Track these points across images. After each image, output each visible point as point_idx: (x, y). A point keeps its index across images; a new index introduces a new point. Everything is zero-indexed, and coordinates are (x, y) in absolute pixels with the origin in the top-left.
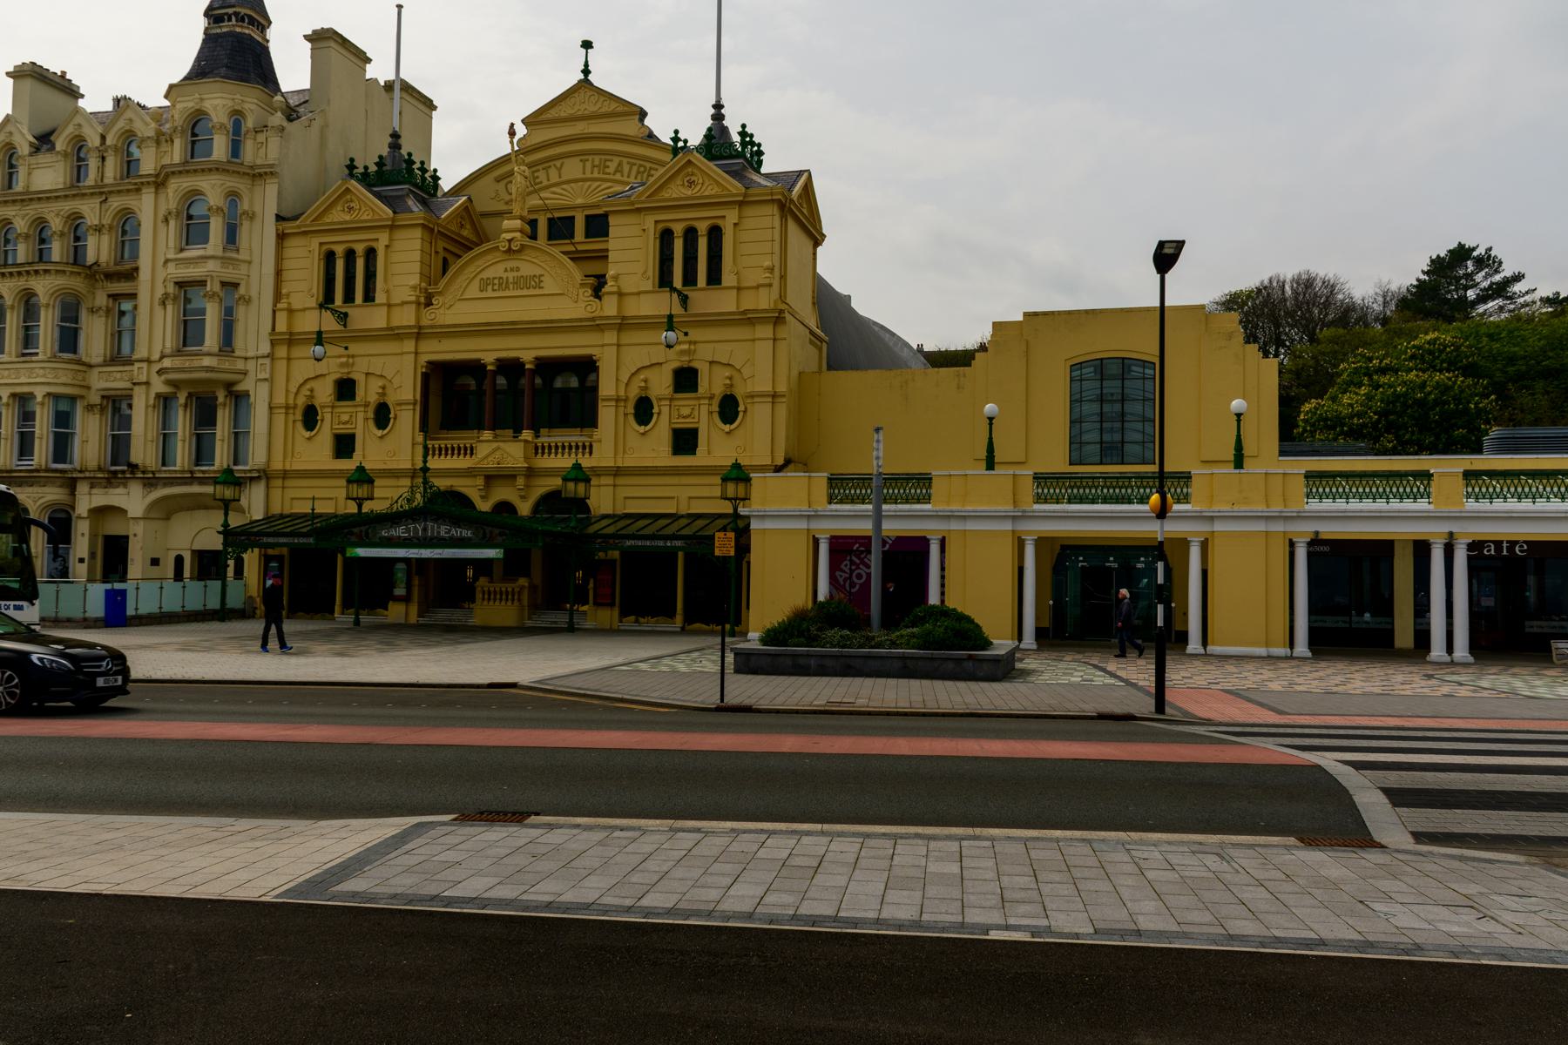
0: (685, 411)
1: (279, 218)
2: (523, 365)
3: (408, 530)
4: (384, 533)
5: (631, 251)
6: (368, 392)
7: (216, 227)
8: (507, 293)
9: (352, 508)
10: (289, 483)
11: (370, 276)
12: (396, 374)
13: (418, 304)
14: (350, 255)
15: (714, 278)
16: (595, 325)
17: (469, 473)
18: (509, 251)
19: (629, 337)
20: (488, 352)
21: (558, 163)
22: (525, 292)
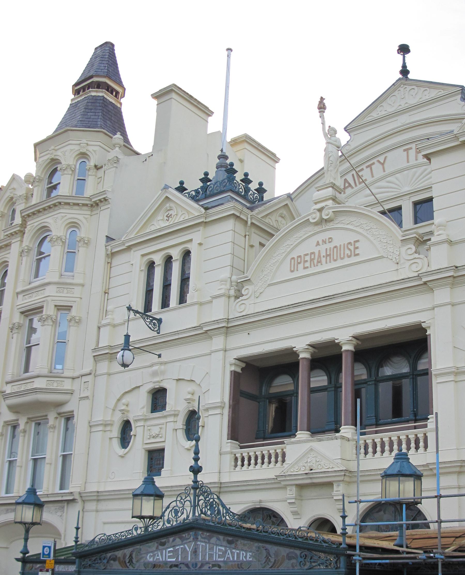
0: (155, 431)
1: (109, 239)
2: (338, 346)
4: (149, 559)
6: (177, 403)
8: (320, 268)
10: (103, 506)
12: (207, 380)
17: (277, 484)
20: (300, 338)
21: (381, 159)
22: (339, 263)
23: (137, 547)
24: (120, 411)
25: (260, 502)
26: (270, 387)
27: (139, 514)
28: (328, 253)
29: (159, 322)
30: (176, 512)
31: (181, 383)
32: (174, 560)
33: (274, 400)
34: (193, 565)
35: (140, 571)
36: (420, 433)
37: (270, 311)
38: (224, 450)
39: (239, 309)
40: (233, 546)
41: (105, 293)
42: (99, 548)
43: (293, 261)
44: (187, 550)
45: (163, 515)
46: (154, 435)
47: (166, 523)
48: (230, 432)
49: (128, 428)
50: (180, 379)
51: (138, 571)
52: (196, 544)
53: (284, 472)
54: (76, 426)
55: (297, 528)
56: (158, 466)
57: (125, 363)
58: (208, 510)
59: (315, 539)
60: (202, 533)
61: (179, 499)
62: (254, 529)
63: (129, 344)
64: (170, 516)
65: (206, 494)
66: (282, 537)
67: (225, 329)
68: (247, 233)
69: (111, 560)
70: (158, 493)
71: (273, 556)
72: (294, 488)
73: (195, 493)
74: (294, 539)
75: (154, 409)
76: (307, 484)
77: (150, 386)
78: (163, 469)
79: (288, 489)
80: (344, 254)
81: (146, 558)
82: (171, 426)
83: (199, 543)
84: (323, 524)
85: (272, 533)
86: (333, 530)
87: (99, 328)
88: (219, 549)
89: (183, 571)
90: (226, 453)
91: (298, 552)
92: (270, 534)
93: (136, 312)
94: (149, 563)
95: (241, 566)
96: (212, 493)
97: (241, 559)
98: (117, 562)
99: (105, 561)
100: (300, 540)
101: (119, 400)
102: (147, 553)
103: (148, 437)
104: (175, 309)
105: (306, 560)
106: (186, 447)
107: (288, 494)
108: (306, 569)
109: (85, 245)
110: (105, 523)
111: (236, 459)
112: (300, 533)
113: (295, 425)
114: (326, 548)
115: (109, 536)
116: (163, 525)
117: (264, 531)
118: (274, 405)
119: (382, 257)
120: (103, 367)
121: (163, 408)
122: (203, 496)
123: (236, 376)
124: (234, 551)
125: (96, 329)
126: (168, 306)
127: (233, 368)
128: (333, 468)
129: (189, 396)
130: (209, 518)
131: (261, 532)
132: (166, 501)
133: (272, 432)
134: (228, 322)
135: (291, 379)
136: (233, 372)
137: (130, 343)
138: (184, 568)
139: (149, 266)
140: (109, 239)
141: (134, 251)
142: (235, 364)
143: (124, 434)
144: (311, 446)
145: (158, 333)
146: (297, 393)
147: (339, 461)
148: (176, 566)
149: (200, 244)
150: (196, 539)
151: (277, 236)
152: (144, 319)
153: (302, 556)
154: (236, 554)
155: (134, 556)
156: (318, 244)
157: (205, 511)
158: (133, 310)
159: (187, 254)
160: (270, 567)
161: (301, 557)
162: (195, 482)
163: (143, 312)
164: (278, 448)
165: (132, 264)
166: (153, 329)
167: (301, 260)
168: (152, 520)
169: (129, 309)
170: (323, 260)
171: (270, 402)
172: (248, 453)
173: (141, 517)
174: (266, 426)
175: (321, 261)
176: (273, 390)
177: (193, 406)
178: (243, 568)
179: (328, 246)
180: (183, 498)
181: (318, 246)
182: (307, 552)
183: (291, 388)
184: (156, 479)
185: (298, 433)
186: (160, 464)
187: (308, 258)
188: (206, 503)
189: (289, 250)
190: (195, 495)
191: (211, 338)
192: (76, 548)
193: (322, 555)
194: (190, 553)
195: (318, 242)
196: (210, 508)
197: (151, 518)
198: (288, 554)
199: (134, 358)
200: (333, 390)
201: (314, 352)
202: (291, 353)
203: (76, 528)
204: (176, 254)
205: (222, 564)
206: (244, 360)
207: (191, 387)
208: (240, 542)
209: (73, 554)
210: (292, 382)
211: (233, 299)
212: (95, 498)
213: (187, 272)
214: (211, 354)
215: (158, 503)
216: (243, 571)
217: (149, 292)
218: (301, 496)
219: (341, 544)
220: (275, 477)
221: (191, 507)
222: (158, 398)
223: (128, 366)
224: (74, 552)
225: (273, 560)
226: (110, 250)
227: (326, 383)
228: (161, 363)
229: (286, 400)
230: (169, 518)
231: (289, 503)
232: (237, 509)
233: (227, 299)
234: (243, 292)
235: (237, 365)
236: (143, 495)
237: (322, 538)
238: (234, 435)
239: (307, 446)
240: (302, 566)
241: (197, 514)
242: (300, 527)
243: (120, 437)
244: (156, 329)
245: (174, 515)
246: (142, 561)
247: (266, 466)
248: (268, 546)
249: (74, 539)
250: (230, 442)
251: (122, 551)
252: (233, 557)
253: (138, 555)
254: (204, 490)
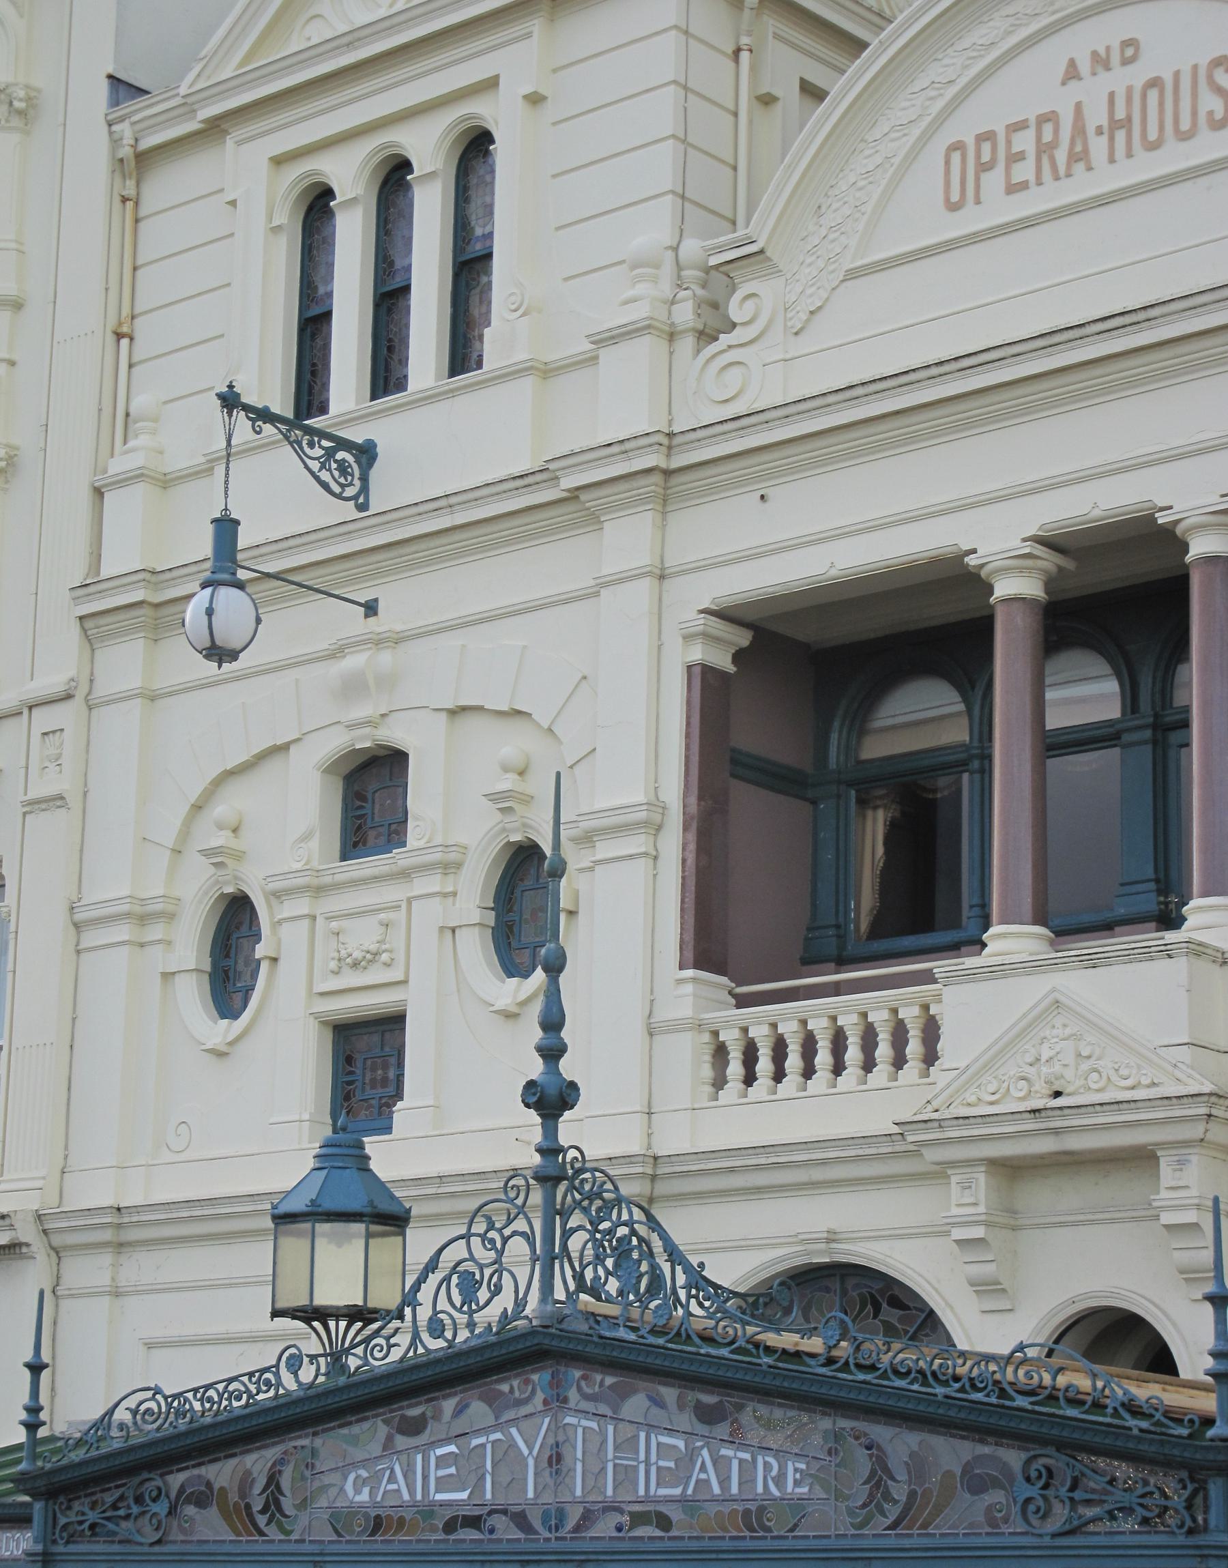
1: (122, 89)
3: (468, 1463)
6: (458, 816)
10: (141, 1268)
11: (470, 267)
17: (904, 1156)
20: (995, 509)
23: (300, 1443)
24: (206, 853)
25: (832, 1237)
26: (862, 732)
27: (303, 1301)
28: (1120, 114)
29: (364, 460)
30: (469, 1285)
31: (472, 723)
32: (464, 1495)
33: (882, 792)
34: (546, 1517)
35: (315, 1548)
37: (860, 391)
38: (664, 1013)
39: (712, 389)
40: (722, 1430)
41: (119, 336)
42: (132, 1449)
43: (956, 157)
44: (521, 1453)
45: (410, 1299)
46: (357, 954)
47: (425, 1336)
48: (690, 936)
49: (244, 929)
50: (464, 709)
51: (307, 1547)
52: (556, 1426)
53: (935, 1104)
54: (12, 928)
55: (1006, 1351)
56: (380, 1091)
57: (218, 642)
58: (608, 1273)
59: (1089, 1399)
60: (584, 1377)
61: (479, 1227)
62: (812, 1356)
63: (234, 561)
64: (443, 1304)
65: (598, 1203)
66: (940, 1390)
67: (657, 478)
68: (745, 40)
69: (188, 1501)
70: (384, 1206)
71: (902, 1476)
72: (981, 1178)
73: (550, 1199)
74: (993, 1400)
75: (355, 845)
76: (1042, 1157)
77: (334, 743)
78: (399, 1105)
79: (954, 1179)
80: (1194, 113)
81: (342, 1489)
82: (429, 915)
83: (568, 1420)
84: (1118, 1335)
85: (896, 1372)
86: (1161, 1361)
87: (99, 493)
88: (659, 1444)
89: (504, 1547)
90: (675, 1027)
91: (1014, 1458)
92: (884, 1376)
93: (263, 415)
94: (353, 1512)
95: (760, 1520)
96: (618, 1201)
97: (760, 1489)
98: (213, 1512)
99: (161, 1508)
100: (1021, 1402)
101: (197, 808)
102: (344, 1470)
103: (333, 965)
104: (428, 398)
105: (1050, 1493)
106: (500, 1004)
107: (954, 1202)
108: (1054, 1536)
109: (16, 122)
110: (150, 1346)
111: (720, 1052)
112: (1021, 1372)
113: (976, 901)
114: (1139, 1440)
115: (175, 1396)
116: (413, 1343)
117: (858, 1366)
118: (881, 814)
120: (124, 664)
121: (395, 834)
122: (586, 1210)
123: (711, 691)
124: (726, 1452)
125: (85, 497)
126: (401, 385)
127: (697, 654)
128: (1154, 1084)
129: (507, 783)
130: (613, 1310)
131: (846, 1367)
132: (420, 1243)
133: (878, 930)
134: (670, 448)
135: (954, 696)
136: (697, 670)
137: (240, 556)
138: (506, 1531)
139: (310, 209)
140: (122, 88)
141: (239, 143)
142: (705, 635)
143: (227, 956)
144: (1054, 990)
145: (362, 507)
146: (987, 758)
147: (1185, 1054)
148: (474, 1522)
149: (535, 99)
150: (557, 1401)
151: (883, 46)
152: (296, 444)
153: (1034, 1474)
154: (735, 1464)
155: (285, 1482)
156: (1072, 73)
157: (596, 1278)
158: (247, 408)
159: (476, 147)
160: (888, 1522)
161: (1028, 1479)
162: (551, 1150)
163: (289, 414)
164: (907, 1003)
165: (233, 203)
166: (337, 489)
167: (994, 150)
168: (359, 1324)
169: (230, 401)
170: (1099, 146)
171: (863, 803)
172: (774, 1026)
173: (312, 1314)
174: (847, 905)
175: (1086, 151)
176: (875, 749)
177: (525, 825)
178: (769, 1530)
179: (1120, 79)
180: (498, 1225)
181: (1073, 84)
182: (1056, 1461)
183: (958, 734)
184: (372, 1145)
185: (991, 931)
186: (385, 1082)
188: (598, 1245)
189: (940, 104)
190: (553, 1212)
191: (594, 520)
192: (34, 1457)
193: (1122, 1470)
194: (531, 1462)
195: (1072, 63)
196: (616, 1265)
197: (357, 1314)
198: (967, 1469)
199: (258, 621)
200: (1145, 742)
201: (1061, 569)
202: (957, 578)
203: (28, 1365)
204: (429, 149)
205: (675, 1514)
206: (750, 617)
207: (512, 743)
208: (752, 1412)
209: (23, 1482)
210: (961, 707)
211: (687, 344)
212: (107, 1235)
213: (479, 232)
214: (597, 594)
215: (386, 1248)
216: (768, 1544)
217: (313, 325)
218: (1012, 1212)
219: (1209, 1422)
220: (896, 1129)
221: (534, 1259)
222: (371, 793)
223: (233, 655)
224: (22, 1473)
225: (900, 1492)
226: (128, 139)
227: (1113, 711)
228: (379, 642)
229: (935, 791)
230: (435, 1313)
231: (958, 1242)
232: (733, 1271)
233: (663, 345)
234: (735, 311)
235: (717, 639)
236: (318, 1214)
237: (1120, 1392)
238: (708, 947)
239: (1036, 989)
240: (1034, 1520)
241: (560, 1294)
242: (1021, 1348)
243: (207, 966)
244: (350, 492)
245: (457, 1300)
246: (323, 1502)
247: (854, 1080)
248: (880, 1432)
249: (23, 1415)
250: (694, 979)
251: (233, 1462)
252: (724, 1482)
253: (303, 1478)
254: (587, 1187)
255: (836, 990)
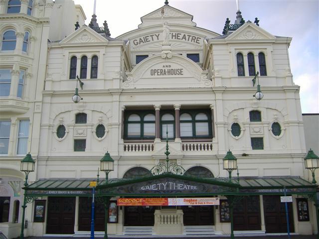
0: (80, 131)
1: (49, 41)
3: (157, 186)
5: (224, 61)
6: (93, 120)
7: (19, 41)
9: (103, 175)
13: (120, 79)
14: (84, 58)
15: (94, 76)
16: (213, 91)
17: (152, 158)
18: (167, 58)
19: (56, 100)
31: (94, 112)
36: (210, 144)
77: (77, 112)
87: (45, 82)
104: (89, 80)
119: (193, 77)
149: (104, 54)
156: (164, 66)
159: (95, 58)
170: (167, 73)
179: (169, 68)
187: (159, 71)
248: (204, 184)
252: (187, 188)
255: (143, 142)
